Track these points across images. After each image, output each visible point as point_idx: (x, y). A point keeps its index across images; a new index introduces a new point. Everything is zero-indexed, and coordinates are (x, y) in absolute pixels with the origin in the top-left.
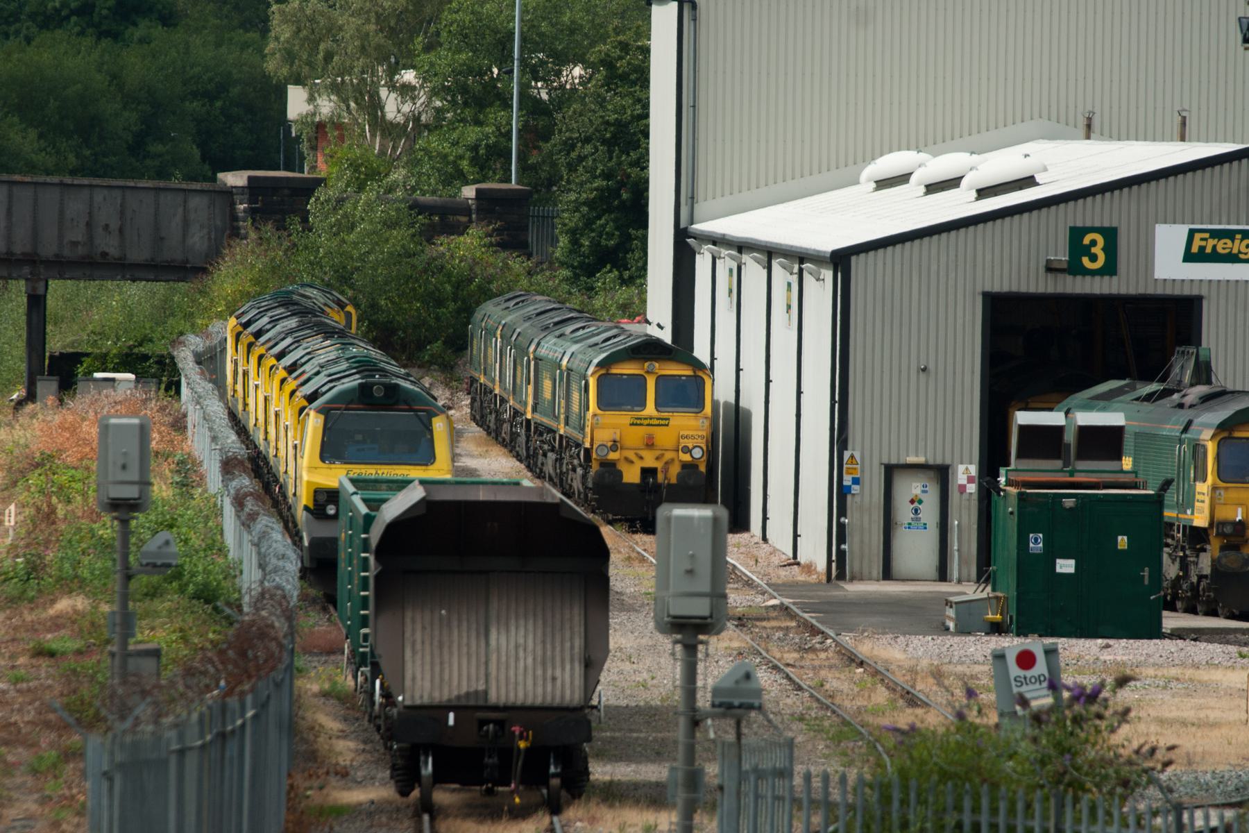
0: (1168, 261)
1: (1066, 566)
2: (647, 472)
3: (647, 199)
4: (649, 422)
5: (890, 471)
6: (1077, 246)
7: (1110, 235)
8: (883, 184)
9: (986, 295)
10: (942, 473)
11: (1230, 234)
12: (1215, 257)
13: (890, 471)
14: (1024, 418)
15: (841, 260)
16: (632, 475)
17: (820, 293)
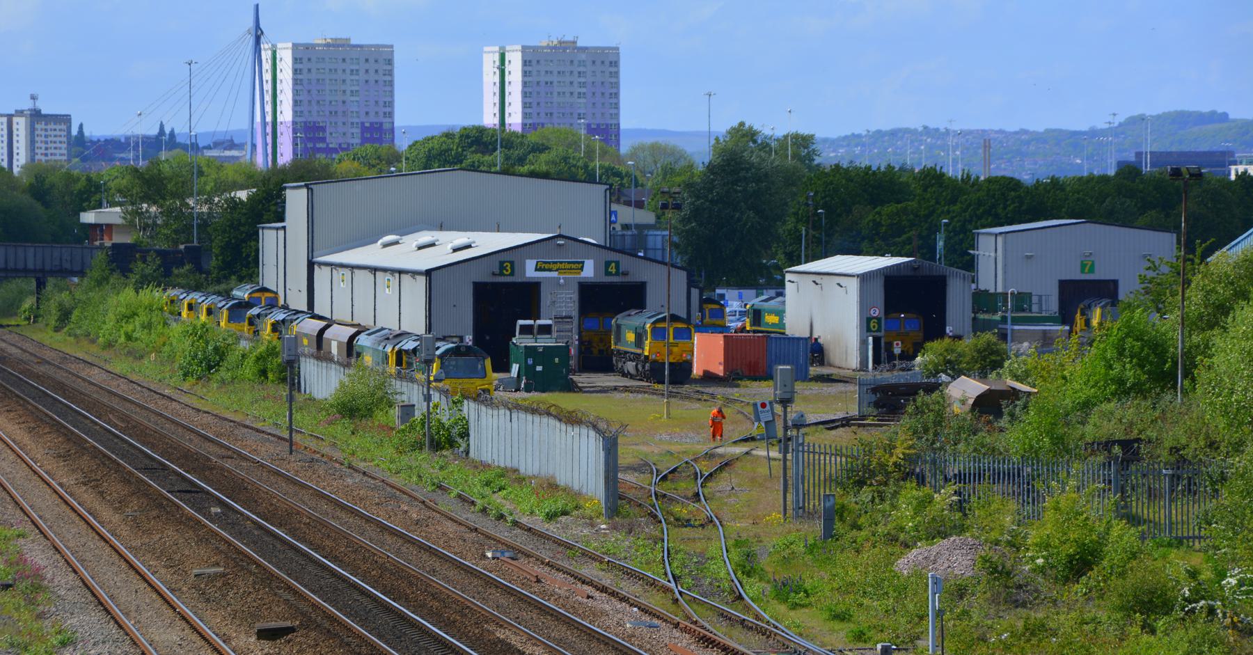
0: (530, 271)
1: (539, 368)
4: (670, 345)
7: (512, 263)
12: (544, 270)
14: (521, 322)
15: (428, 273)
17: (422, 280)
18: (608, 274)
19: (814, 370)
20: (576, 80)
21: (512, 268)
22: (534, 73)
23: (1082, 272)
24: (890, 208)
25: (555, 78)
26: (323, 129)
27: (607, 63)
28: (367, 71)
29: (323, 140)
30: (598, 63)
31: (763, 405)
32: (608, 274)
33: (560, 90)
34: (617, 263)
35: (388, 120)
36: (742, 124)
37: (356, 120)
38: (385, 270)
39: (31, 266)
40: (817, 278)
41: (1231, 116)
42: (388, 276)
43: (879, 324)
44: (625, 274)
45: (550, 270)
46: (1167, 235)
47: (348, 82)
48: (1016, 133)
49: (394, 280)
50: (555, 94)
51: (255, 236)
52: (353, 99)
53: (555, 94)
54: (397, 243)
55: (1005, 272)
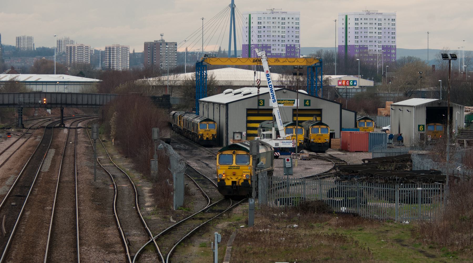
2: (234, 182)
3: (434, 50)
5: (234, 133)
6: (259, 103)
7: (263, 100)
8: (226, 94)
10: (241, 133)
13: (234, 133)
15: (227, 104)
16: (228, 183)
18: (305, 105)
19: (278, 138)
21: (264, 102)
25: (368, 26)
29: (367, 53)
32: (305, 105)
34: (309, 101)
35: (297, 44)
39: (98, 103)
40: (409, 109)
43: (424, 127)
50: (272, 32)
54: (231, 92)
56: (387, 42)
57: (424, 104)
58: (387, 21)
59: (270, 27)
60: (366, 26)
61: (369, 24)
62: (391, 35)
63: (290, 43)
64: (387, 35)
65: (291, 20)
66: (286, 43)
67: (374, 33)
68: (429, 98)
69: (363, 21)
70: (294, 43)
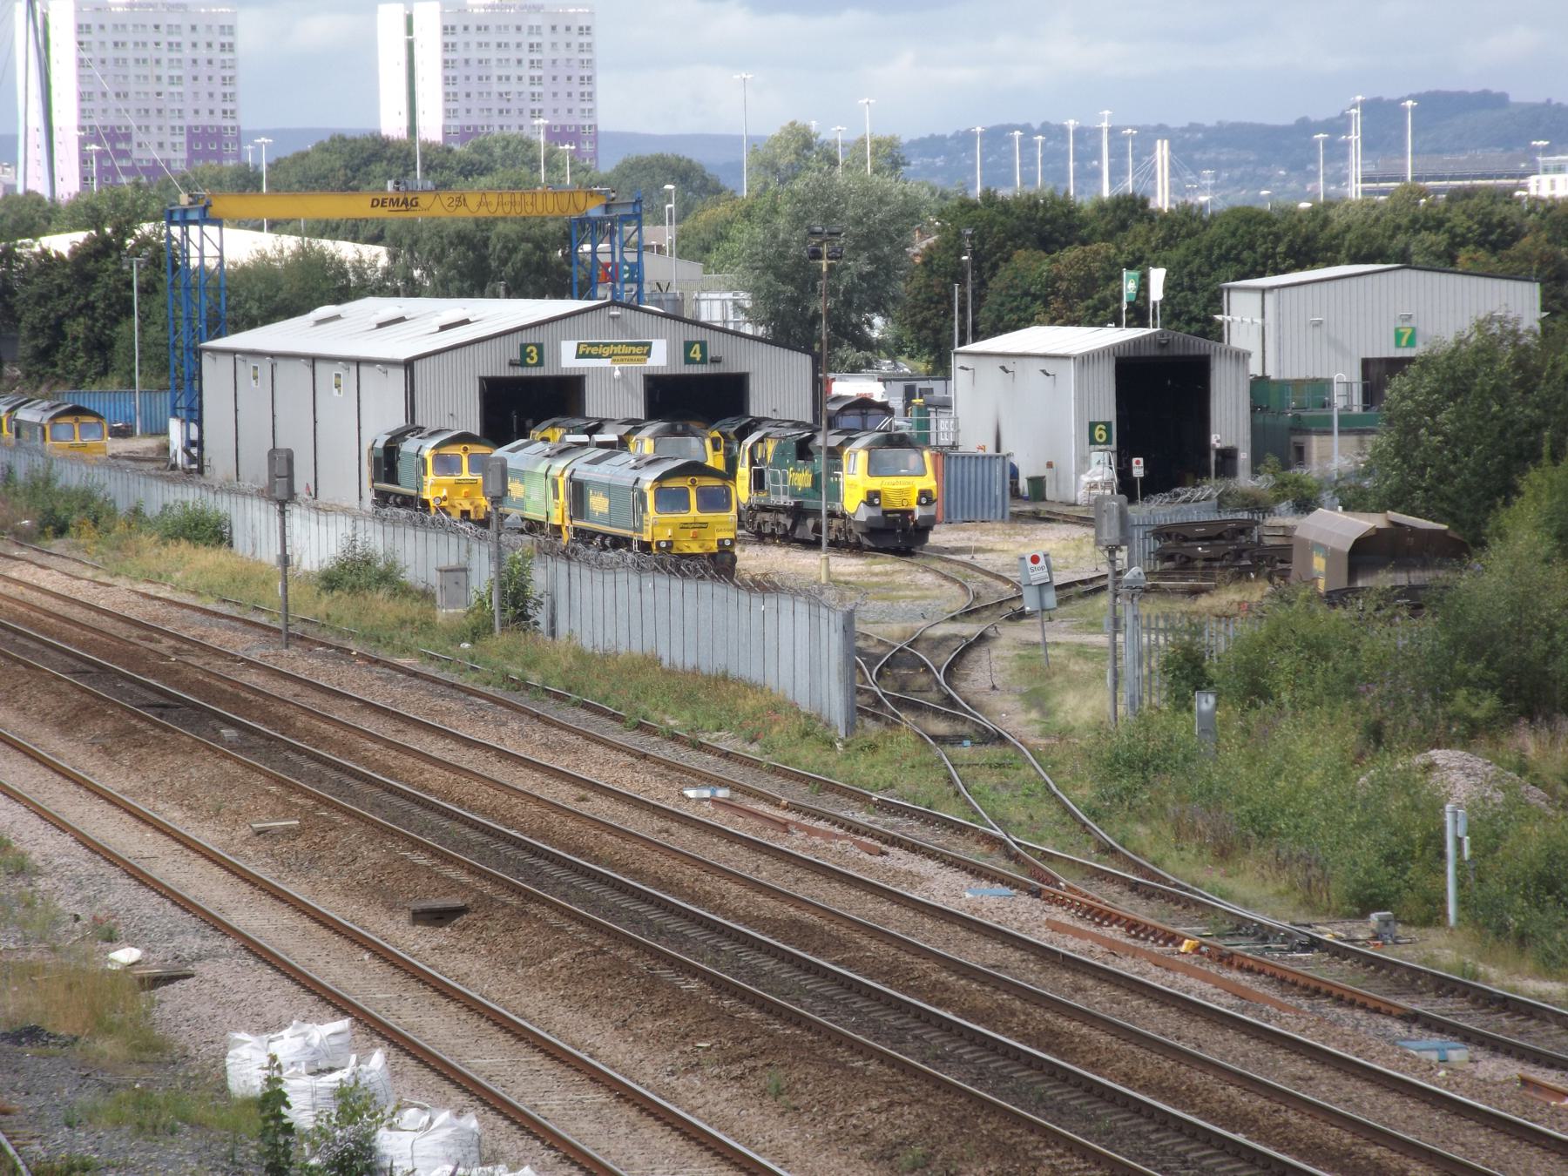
0: (568, 359)
3: (1252, 125)
6: (524, 353)
7: (540, 347)
9: (482, 379)
11: (597, 345)
12: (590, 356)
15: (409, 365)
18: (689, 361)
20: (526, 56)
22: (96, 45)
23: (1398, 345)
24: (1072, 253)
25: (493, 54)
26: (127, 137)
27: (575, 30)
28: (194, 45)
30: (561, 29)
31: (1035, 559)
33: (503, 72)
34: (703, 345)
36: (793, 124)
37: (177, 123)
38: (371, 362)
40: (1049, 366)
41: (1513, 99)
42: (338, 368)
44: (716, 361)
45: (599, 356)
46: (1526, 285)
47: (164, 62)
48: (1182, 130)
49: (349, 378)
51: (1216, 301)
52: (174, 89)
53: (494, 79)
55: (1279, 349)
56: (204, 114)
57: (1108, 348)
58: (561, 37)
59: (125, 61)
60: (484, 55)
61: (493, 46)
62: (577, 89)
63: (204, 120)
64: (562, 87)
65: (561, 37)
66: (190, 120)
67: (514, 80)
68: (540, 295)
69: (474, 37)
70: (218, 120)
